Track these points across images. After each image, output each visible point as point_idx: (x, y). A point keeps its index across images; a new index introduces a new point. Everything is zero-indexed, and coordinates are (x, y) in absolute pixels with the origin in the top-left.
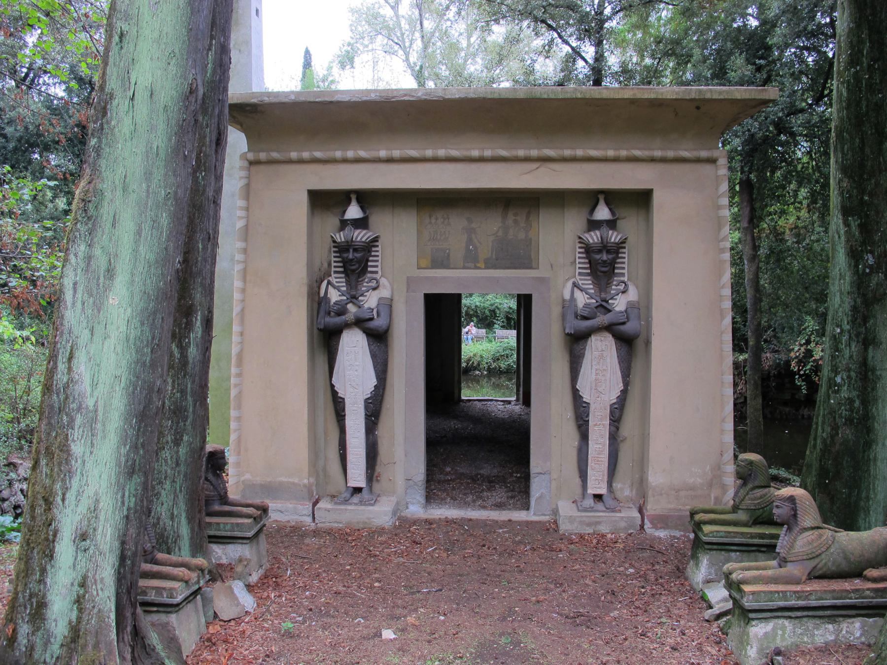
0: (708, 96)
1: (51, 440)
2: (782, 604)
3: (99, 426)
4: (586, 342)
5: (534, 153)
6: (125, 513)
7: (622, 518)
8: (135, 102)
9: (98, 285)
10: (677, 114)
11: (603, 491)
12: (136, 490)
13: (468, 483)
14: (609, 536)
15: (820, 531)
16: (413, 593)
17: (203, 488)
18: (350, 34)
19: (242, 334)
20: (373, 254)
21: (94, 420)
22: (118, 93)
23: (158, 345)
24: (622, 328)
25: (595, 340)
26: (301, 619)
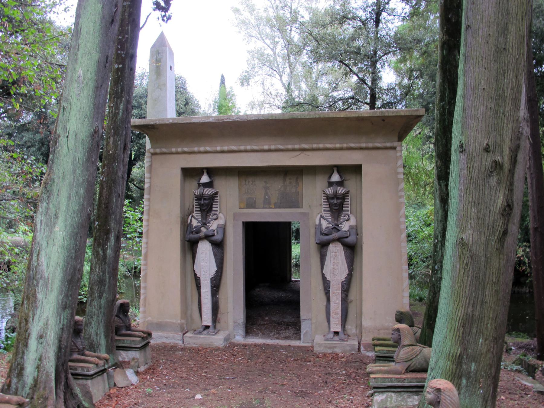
0: (386, 114)
1: (29, 292)
2: (389, 384)
3: (50, 285)
4: (327, 248)
5: (297, 146)
6: (61, 327)
7: (348, 344)
8: (69, 139)
9: (51, 221)
10: (372, 124)
11: (339, 329)
12: (67, 316)
13: (275, 326)
14: (340, 354)
15: (413, 347)
16: (221, 379)
17: (114, 321)
18: (247, 66)
19: (147, 243)
20: (215, 201)
21: (47, 283)
22: (62, 135)
23: (78, 249)
24: (346, 240)
25: (332, 246)
26: (159, 389)
